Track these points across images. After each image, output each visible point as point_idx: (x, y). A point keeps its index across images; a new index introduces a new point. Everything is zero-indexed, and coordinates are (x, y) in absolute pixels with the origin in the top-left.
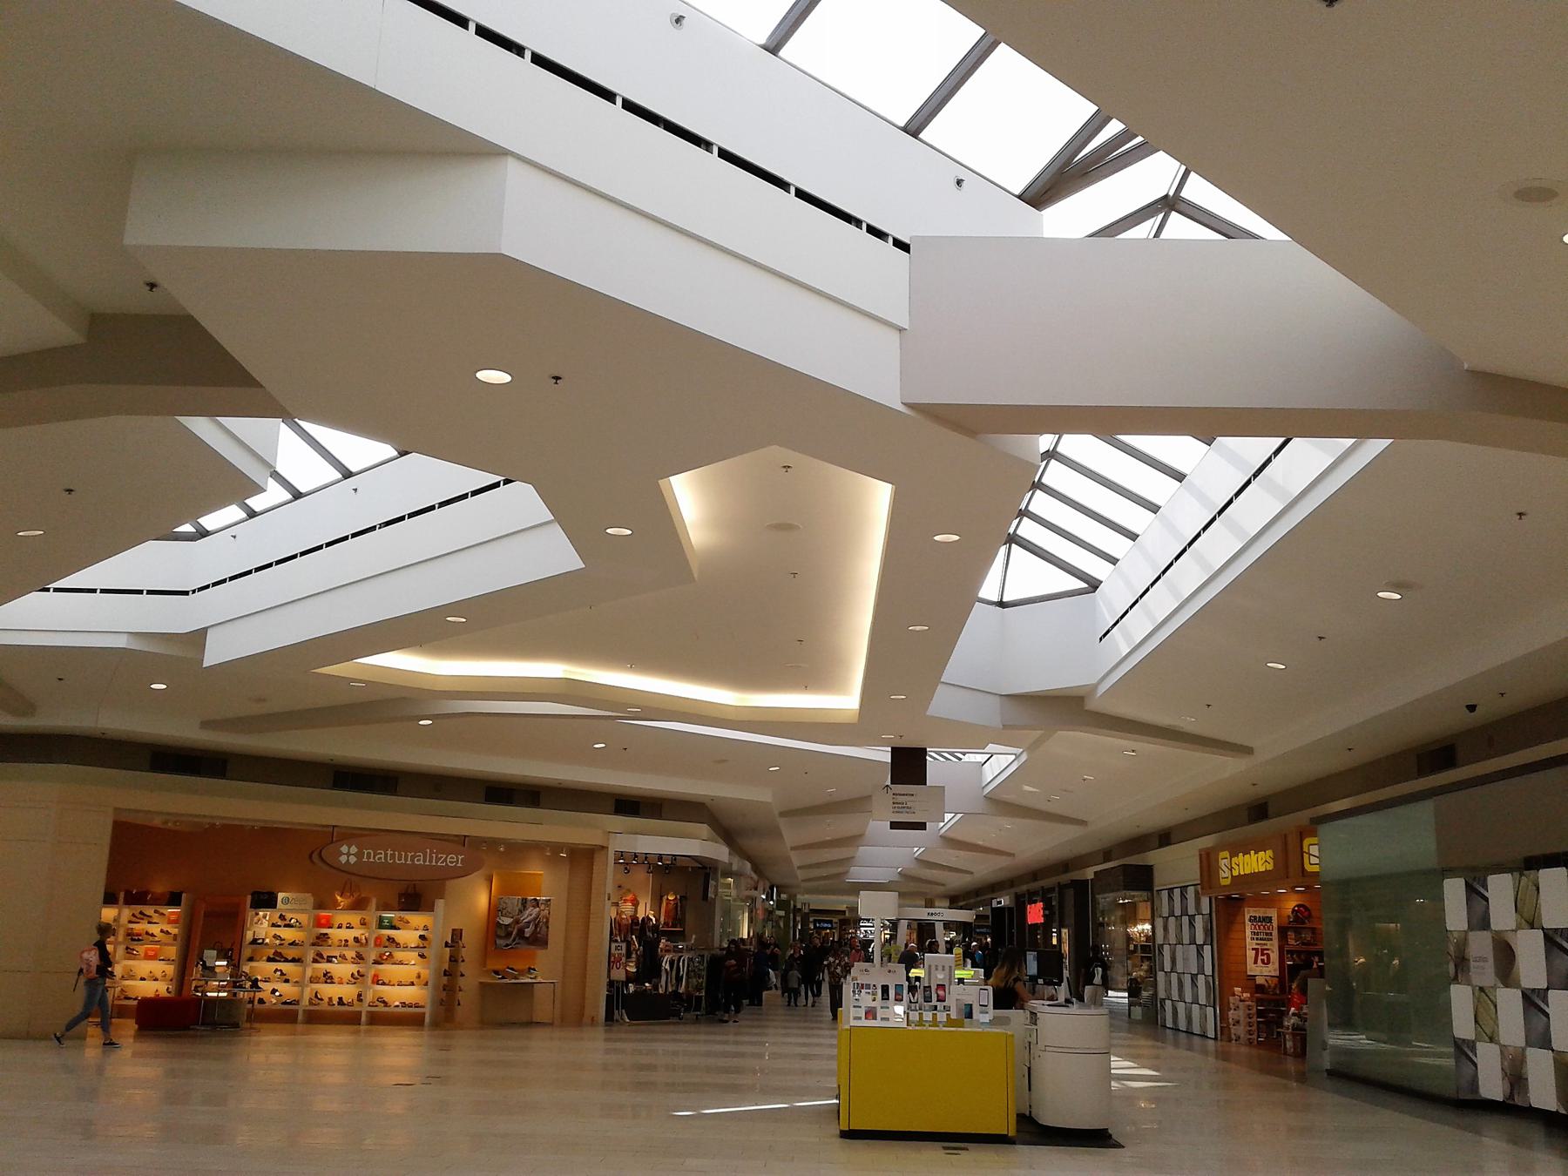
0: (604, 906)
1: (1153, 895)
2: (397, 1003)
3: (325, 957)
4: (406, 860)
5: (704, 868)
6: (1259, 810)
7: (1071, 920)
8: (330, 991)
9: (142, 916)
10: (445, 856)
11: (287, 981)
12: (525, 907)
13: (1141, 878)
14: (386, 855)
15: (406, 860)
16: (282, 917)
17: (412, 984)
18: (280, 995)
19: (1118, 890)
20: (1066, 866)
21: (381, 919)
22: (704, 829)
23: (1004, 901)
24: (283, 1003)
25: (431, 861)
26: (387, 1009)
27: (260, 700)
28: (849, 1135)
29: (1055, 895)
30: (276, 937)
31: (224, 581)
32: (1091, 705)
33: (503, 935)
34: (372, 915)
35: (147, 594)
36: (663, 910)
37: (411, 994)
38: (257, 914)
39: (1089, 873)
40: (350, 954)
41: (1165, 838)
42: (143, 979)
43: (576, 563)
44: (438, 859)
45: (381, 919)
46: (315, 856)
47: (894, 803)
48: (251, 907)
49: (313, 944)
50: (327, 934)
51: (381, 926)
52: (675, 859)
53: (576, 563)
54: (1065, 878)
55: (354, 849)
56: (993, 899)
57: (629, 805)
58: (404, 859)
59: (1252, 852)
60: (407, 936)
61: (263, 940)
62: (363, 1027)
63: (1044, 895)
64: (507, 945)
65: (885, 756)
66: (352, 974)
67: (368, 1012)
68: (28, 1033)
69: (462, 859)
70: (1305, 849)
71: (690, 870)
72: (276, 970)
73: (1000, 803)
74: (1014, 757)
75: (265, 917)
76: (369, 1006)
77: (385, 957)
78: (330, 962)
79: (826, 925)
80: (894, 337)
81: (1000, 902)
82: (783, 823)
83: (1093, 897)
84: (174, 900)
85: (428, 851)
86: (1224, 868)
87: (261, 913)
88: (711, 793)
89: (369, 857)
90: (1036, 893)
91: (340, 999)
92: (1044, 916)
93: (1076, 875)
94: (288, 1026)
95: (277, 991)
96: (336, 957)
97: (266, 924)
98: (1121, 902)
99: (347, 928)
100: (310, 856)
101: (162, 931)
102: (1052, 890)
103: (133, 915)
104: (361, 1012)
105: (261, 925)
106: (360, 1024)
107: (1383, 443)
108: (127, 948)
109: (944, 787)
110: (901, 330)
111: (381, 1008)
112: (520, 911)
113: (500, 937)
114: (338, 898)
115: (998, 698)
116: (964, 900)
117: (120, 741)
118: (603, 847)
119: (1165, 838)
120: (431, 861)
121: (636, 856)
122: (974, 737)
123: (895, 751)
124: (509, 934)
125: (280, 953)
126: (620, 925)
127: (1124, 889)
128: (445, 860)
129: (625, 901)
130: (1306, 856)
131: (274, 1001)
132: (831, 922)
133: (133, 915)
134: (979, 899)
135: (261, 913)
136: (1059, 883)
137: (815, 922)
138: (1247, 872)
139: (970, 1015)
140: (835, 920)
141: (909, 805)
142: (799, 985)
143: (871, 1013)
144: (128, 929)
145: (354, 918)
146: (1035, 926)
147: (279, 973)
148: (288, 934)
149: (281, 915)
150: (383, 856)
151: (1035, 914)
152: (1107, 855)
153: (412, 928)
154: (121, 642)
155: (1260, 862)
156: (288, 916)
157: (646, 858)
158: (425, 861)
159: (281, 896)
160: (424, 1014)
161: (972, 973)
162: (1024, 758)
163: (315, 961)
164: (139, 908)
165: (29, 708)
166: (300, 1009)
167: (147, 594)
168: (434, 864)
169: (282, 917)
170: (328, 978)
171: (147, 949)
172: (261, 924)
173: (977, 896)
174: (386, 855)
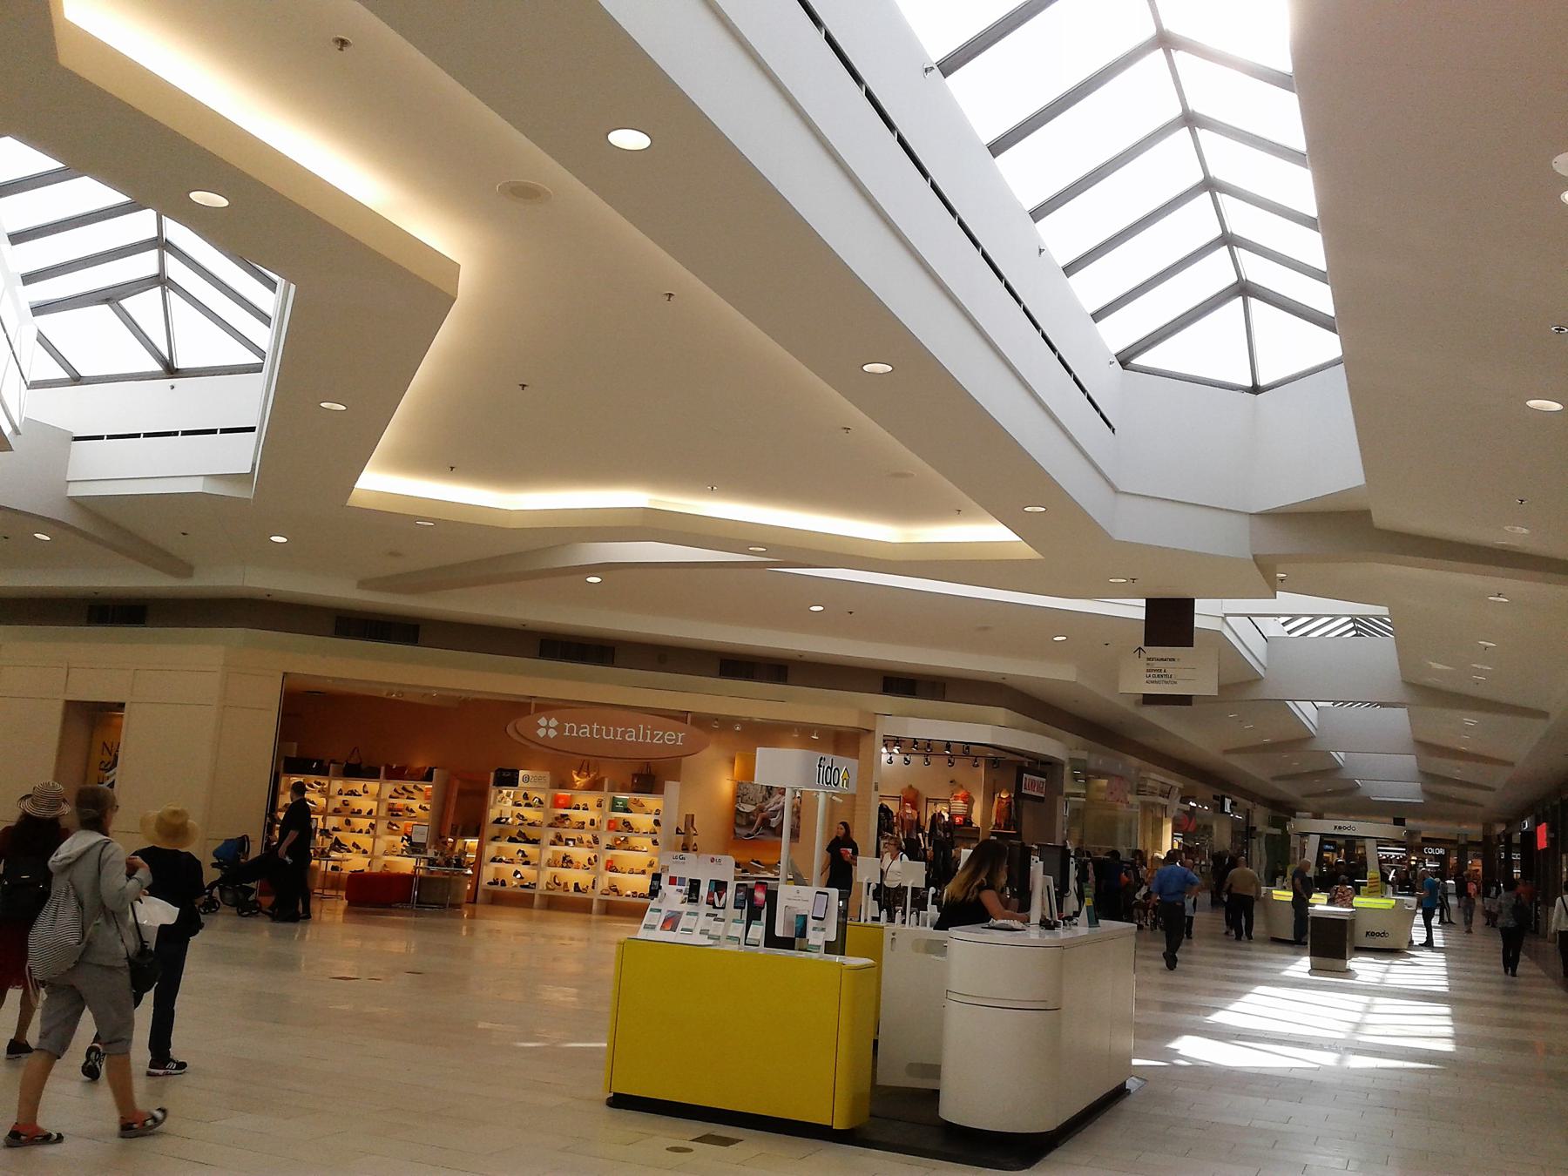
2: (629, 893)
3: (564, 840)
4: (615, 735)
8: (572, 876)
9: (404, 792)
10: (661, 733)
11: (527, 863)
12: (770, 794)
15: (615, 735)
16: (526, 796)
17: (643, 872)
18: (522, 878)
21: (614, 800)
24: (523, 886)
25: (645, 736)
26: (619, 899)
27: (394, 554)
28: (620, 1101)
30: (519, 816)
33: (744, 824)
34: (606, 797)
35: (221, 433)
36: (995, 808)
38: (501, 792)
40: (587, 837)
42: (632, 872)
44: (653, 737)
45: (614, 800)
47: (1148, 671)
49: (551, 826)
50: (567, 815)
51: (614, 809)
52: (968, 748)
55: (553, 722)
60: (642, 821)
61: (507, 819)
62: (594, 917)
64: (749, 835)
65: (1135, 610)
66: (589, 859)
72: (520, 851)
75: (508, 795)
76: (602, 894)
77: (619, 842)
78: (567, 844)
84: (428, 777)
85: (642, 726)
87: (505, 792)
88: (1033, 674)
91: (576, 885)
94: (583, 916)
95: (519, 872)
96: (573, 840)
97: (510, 803)
99: (584, 809)
101: (420, 807)
103: (395, 790)
105: (503, 804)
106: (591, 913)
108: (390, 823)
111: (613, 897)
112: (765, 799)
113: (740, 826)
114: (575, 776)
115: (1248, 517)
117: (306, 605)
118: (869, 731)
120: (645, 736)
121: (916, 743)
124: (750, 824)
125: (524, 834)
126: (903, 821)
128: (662, 737)
129: (956, 798)
131: (515, 883)
133: (395, 790)
135: (505, 792)
139: (802, 932)
141: (1169, 672)
142: (927, 888)
143: (672, 922)
144: (390, 804)
145: (590, 799)
147: (520, 854)
148: (531, 814)
149: (525, 794)
150: (587, 730)
154: (197, 486)
156: (532, 794)
157: (929, 746)
158: (637, 737)
159: (522, 773)
161: (1394, 902)
163: (553, 843)
164: (401, 783)
165: (183, 568)
166: (537, 892)
167: (221, 433)
168: (648, 741)
169: (526, 796)
170: (567, 862)
171: (406, 826)
172: (505, 802)
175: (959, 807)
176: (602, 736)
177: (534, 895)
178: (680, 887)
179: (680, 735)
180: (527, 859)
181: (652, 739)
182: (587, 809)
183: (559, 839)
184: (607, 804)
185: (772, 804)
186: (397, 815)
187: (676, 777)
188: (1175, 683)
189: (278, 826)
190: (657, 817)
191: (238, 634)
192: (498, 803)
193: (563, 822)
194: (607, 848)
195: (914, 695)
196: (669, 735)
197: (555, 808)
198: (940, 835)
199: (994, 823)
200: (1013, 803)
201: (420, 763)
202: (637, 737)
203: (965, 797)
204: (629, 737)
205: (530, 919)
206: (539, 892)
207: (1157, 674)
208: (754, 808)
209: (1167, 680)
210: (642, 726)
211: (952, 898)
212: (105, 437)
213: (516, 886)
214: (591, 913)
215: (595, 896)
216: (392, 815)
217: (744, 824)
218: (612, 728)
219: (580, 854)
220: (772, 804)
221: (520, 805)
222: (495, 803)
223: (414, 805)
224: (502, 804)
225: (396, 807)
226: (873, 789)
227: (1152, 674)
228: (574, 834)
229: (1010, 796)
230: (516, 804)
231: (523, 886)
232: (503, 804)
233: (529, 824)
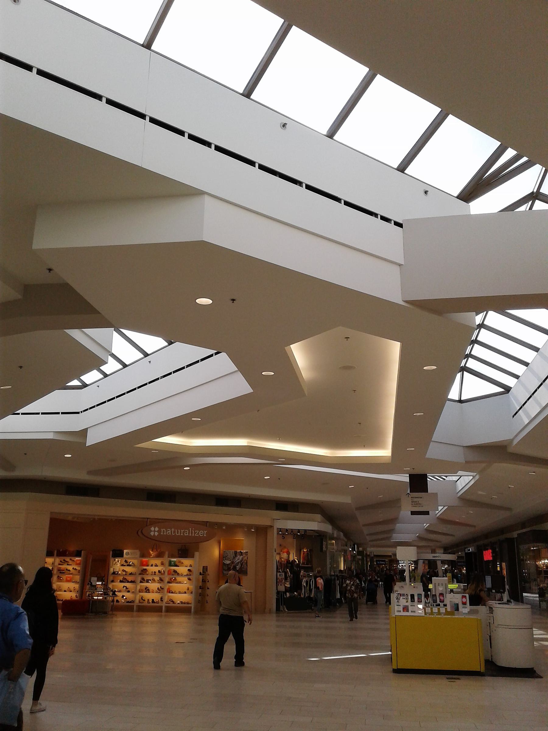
2: (179, 602)
11: (129, 592)
17: (185, 593)
18: (126, 598)
22: (319, 517)
25: (192, 534)
26: (174, 605)
30: (123, 571)
32: (510, 450)
34: (166, 560)
37: (185, 597)
40: (157, 578)
44: (195, 533)
45: (170, 562)
46: (139, 533)
49: (140, 574)
50: (146, 569)
51: (170, 565)
52: (306, 532)
55: (157, 529)
56: (465, 548)
58: (180, 533)
60: (182, 570)
61: (118, 572)
62: (163, 614)
63: (492, 546)
65: (405, 478)
72: (124, 586)
75: (118, 561)
76: (166, 603)
80: (398, 268)
84: (78, 554)
85: (190, 529)
91: (153, 600)
92: (492, 556)
93: (508, 536)
95: (124, 596)
99: (155, 566)
100: (137, 533)
101: (73, 568)
105: (117, 565)
110: (400, 265)
111: (171, 604)
112: (234, 558)
120: (192, 534)
126: (281, 564)
129: (284, 552)
131: (123, 601)
132: (384, 561)
137: (377, 561)
139: (457, 609)
140: (386, 560)
145: (158, 561)
146: (488, 562)
148: (129, 569)
150: (170, 532)
151: (488, 555)
152: (523, 525)
154: (50, 436)
156: (129, 561)
157: (292, 531)
158: (189, 534)
159: (125, 551)
161: (457, 585)
162: (477, 477)
163: (141, 582)
167: (61, 414)
169: (126, 561)
170: (147, 590)
172: (117, 565)
175: (285, 555)
176: (175, 534)
177: (134, 606)
178: (403, 597)
179: (205, 532)
180: (128, 590)
182: (157, 566)
183: (143, 580)
184: (167, 564)
185: (236, 560)
186: (63, 573)
187: (197, 550)
188: (423, 506)
190: (189, 568)
191: (27, 495)
192: (114, 565)
193: (146, 572)
194: (167, 583)
195: (287, 510)
196: (201, 532)
197: (170, 566)
198: (296, 569)
199: (302, 563)
200: (309, 554)
201: (72, 548)
203: (287, 552)
204: (164, 530)
205: (132, 617)
206: (136, 604)
207: (415, 503)
208: (230, 562)
209: (419, 505)
210: (190, 529)
211: (470, 594)
213: (124, 602)
214: (162, 612)
215: (164, 605)
216: (61, 573)
217: (226, 569)
218: (179, 530)
219: (154, 586)
220: (236, 560)
221: (125, 566)
222: (112, 565)
223: (70, 568)
224: (116, 565)
225: (62, 569)
226: (274, 551)
227: (413, 503)
228: (150, 578)
229: (307, 550)
230: (122, 565)
231: (128, 602)
232: (117, 565)
233: (130, 574)
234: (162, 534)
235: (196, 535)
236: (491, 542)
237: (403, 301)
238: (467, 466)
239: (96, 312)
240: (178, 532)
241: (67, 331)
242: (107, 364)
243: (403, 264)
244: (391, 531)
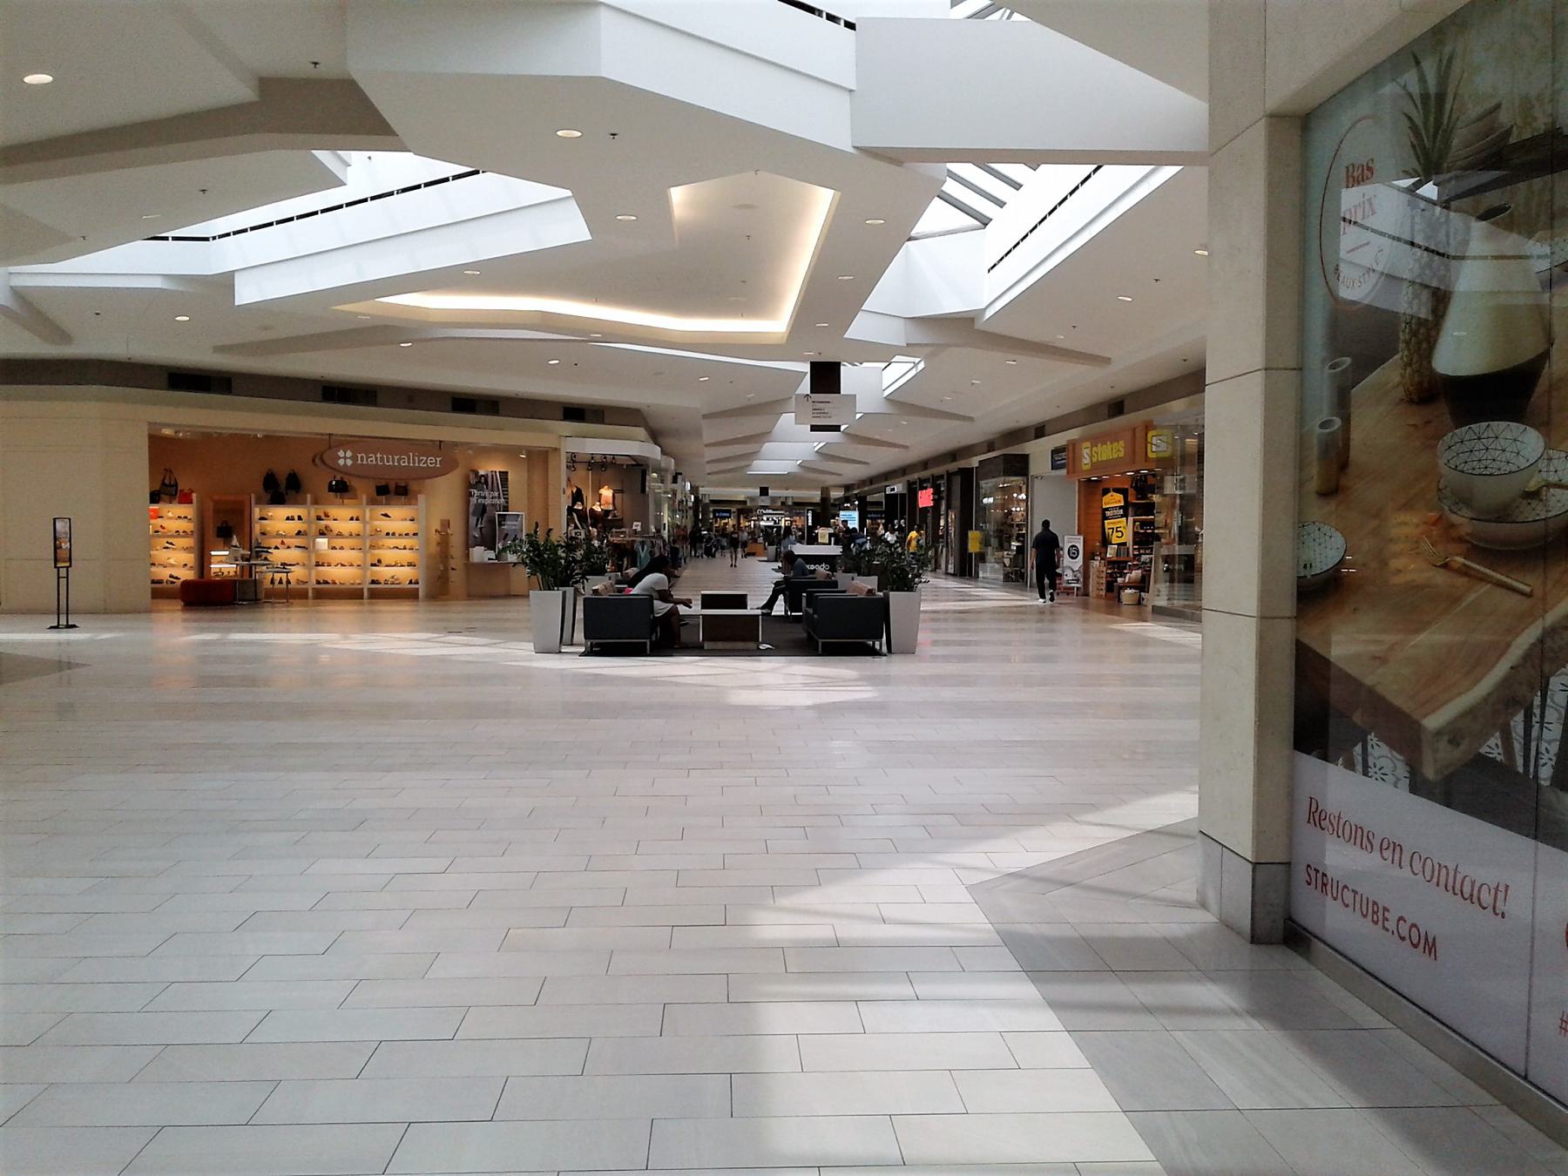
0: (560, 498)
1: (1028, 479)
5: (638, 465)
6: (1116, 407)
7: (956, 502)
10: (425, 458)
13: (1018, 466)
14: (376, 458)
19: (999, 476)
20: (953, 455)
22: (641, 432)
23: (898, 488)
25: (414, 463)
27: (266, 328)
29: (942, 482)
31: (245, 231)
32: (978, 325)
37: (404, 574)
39: (974, 462)
41: (1040, 431)
43: (585, 235)
46: (317, 461)
48: (256, 503)
53: (585, 235)
54: (953, 466)
55: (349, 454)
57: (575, 413)
58: (392, 461)
59: (1108, 443)
62: (365, 601)
63: (934, 482)
67: (369, 589)
68: (105, 609)
69: (440, 461)
70: (1149, 440)
71: (625, 467)
73: (902, 403)
74: (912, 365)
79: (724, 514)
80: (846, 97)
81: (893, 489)
82: (704, 423)
83: (978, 484)
85: (411, 454)
86: (1086, 456)
89: (362, 460)
90: (926, 480)
93: (962, 464)
98: (1001, 486)
100: (314, 461)
102: (941, 477)
104: (362, 589)
107: (1176, 169)
109: (855, 395)
110: (851, 91)
116: (858, 488)
118: (556, 449)
119: (1040, 431)
120: (414, 463)
122: (883, 353)
123: (813, 364)
127: (1004, 475)
130: (1149, 445)
132: (729, 511)
134: (873, 486)
136: (947, 471)
137: (714, 512)
138: (1104, 459)
140: (733, 510)
146: (925, 509)
150: (374, 459)
151: (925, 499)
152: (990, 446)
153: (397, 518)
154: (157, 284)
155: (1114, 451)
158: (409, 463)
160: (418, 589)
162: (921, 366)
173: (871, 484)
174: (376, 458)
181: (419, 463)
189: (805, 594)
202: (409, 463)
204: (362, 457)
210: (411, 454)
212: (423, 186)
234: (359, 462)
235: (421, 465)
236: (919, 478)
237: (854, 147)
238: (909, 349)
239: (393, 133)
240: (388, 458)
241: (317, 153)
242: (343, 187)
243: (854, 88)
244: (753, 455)
